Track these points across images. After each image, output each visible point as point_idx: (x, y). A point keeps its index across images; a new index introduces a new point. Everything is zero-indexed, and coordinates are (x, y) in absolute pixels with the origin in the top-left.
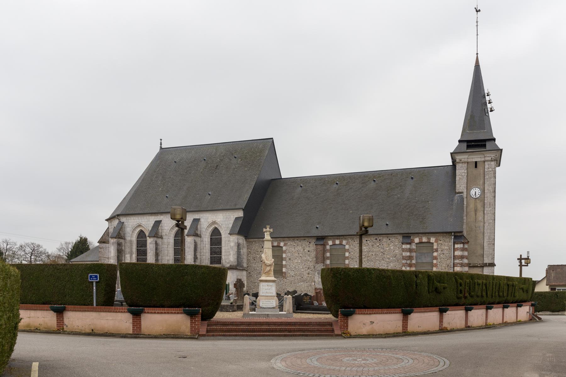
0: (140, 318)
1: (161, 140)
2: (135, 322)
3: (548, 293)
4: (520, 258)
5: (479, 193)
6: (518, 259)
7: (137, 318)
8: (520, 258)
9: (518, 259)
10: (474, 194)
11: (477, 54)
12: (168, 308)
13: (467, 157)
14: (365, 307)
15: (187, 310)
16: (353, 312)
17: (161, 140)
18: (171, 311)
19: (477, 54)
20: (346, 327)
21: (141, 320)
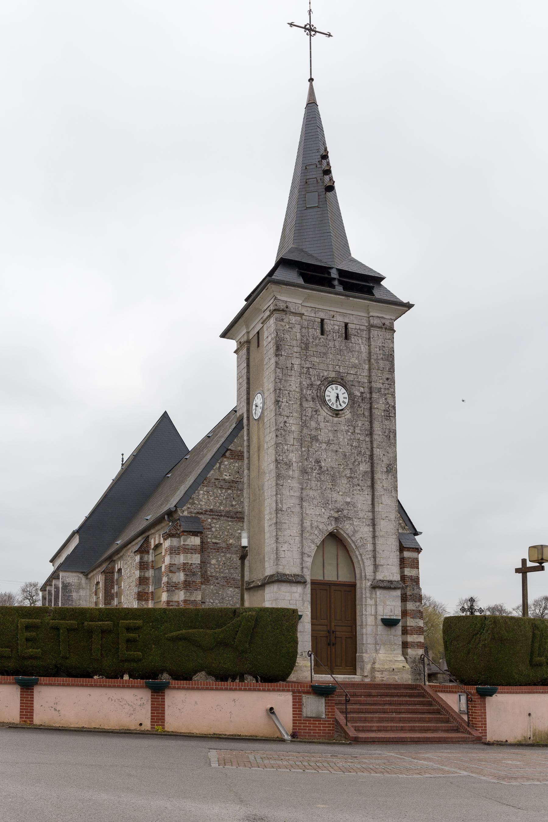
0: (33, 692)
1: (123, 455)
2: (29, 700)
3: (515, 618)
4: (520, 566)
5: (334, 388)
6: (517, 571)
7: (28, 692)
8: (520, 566)
9: (517, 571)
10: (333, 399)
11: (311, 80)
12: (45, 678)
13: (300, 302)
14: (509, 684)
15: (150, 684)
16: (493, 691)
17: (123, 455)
18: (183, 685)
19: (311, 80)
20: (29, 700)
21: (33, 695)
